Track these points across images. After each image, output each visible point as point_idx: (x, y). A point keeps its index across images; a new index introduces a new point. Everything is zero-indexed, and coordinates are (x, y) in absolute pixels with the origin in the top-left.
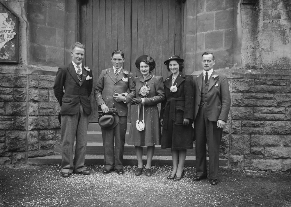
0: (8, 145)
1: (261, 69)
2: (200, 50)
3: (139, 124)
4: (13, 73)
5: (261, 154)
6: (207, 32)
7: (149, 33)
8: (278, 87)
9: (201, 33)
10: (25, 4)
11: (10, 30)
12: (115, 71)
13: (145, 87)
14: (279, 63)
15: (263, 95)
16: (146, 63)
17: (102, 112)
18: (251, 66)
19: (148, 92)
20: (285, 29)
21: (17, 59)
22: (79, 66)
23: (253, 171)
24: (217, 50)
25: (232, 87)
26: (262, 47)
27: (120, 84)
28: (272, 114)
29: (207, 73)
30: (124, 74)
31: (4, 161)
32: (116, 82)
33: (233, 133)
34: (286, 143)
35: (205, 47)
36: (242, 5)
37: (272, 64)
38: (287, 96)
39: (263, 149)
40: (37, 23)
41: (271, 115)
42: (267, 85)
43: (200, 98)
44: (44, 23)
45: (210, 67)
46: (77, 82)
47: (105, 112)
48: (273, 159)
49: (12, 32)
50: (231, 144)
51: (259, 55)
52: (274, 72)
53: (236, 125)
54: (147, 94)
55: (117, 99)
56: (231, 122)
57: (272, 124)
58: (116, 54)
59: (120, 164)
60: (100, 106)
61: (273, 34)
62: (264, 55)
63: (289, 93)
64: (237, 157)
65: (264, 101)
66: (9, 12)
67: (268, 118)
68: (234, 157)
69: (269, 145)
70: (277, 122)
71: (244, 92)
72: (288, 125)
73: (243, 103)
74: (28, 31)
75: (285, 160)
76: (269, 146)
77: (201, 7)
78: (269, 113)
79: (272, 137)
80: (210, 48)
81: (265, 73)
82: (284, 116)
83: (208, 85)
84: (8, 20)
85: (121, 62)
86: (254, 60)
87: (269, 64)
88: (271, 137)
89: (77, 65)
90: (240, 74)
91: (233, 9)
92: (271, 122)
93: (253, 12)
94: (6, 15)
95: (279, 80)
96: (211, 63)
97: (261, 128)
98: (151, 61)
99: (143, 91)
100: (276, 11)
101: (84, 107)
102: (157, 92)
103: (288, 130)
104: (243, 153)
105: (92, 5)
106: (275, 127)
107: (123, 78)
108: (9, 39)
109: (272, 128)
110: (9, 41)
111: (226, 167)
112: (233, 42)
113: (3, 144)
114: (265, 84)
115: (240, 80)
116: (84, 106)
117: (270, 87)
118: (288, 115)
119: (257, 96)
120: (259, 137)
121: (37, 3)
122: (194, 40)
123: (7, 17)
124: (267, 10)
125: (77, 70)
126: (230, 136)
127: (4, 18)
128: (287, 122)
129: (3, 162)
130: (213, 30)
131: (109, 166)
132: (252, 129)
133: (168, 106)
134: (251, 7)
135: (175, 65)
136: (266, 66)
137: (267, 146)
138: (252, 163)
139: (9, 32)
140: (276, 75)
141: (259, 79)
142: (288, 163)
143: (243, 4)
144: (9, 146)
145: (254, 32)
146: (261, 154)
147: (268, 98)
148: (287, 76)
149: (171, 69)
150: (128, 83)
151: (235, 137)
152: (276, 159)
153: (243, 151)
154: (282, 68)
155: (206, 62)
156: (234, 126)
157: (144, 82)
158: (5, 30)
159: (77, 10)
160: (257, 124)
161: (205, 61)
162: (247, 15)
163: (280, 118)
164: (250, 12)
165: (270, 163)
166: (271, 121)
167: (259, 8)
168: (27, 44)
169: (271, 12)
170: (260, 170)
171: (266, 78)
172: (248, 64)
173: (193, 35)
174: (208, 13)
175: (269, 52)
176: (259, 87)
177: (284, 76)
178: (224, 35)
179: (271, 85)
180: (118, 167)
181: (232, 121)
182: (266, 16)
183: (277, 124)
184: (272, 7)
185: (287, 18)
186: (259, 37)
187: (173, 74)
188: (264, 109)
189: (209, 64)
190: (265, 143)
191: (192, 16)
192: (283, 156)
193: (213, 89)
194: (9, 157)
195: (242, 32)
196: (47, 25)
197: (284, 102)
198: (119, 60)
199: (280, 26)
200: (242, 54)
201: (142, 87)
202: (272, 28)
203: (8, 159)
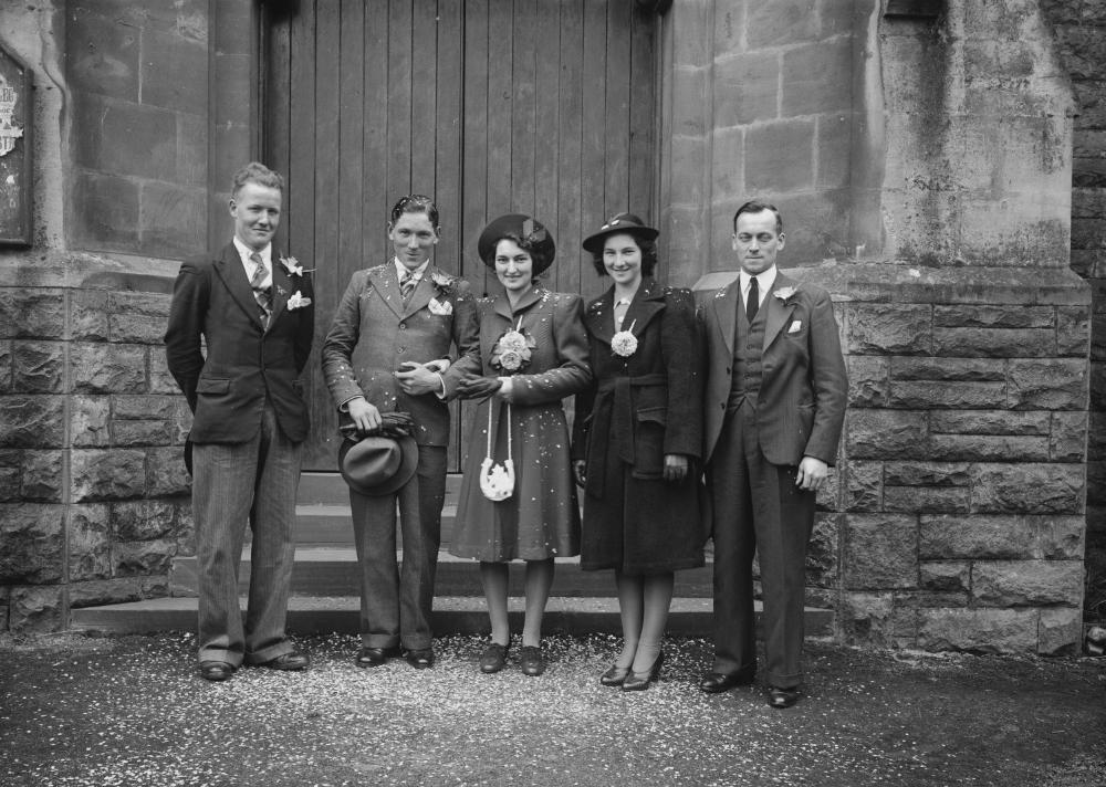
1: (959, 264)
2: (723, 194)
3: (490, 473)
4: (13, 283)
5: (960, 588)
6: (751, 126)
7: (530, 128)
8: (1023, 334)
9: (727, 129)
10: (56, 20)
12: (401, 273)
13: (513, 336)
14: (1028, 241)
15: (965, 365)
16: (519, 245)
17: (356, 429)
18: (918, 255)
19: (527, 355)
20: (1049, 112)
22: (261, 254)
23: (929, 655)
24: (791, 195)
25: (849, 336)
27: (422, 324)
28: (1002, 438)
29: (754, 282)
30: (435, 284)
32: (403, 317)
33: (853, 511)
35: (743, 184)
36: (885, 24)
37: (1000, 248)
38: (1056, 368)
39: (968, 570)
40: (101, 91)
43: (730, 377)
45: (769, 258)
46: (254, 316)
47: (368, 427)
50: (845, 551)
51: (948, 213)
52: (1008, 276)
53: (861, 479)
54: (523, 361)
55: (409, 382)
56: (843, 468)
57: (999, 474)
58: (409, 211)
60: (346, 406)
61: (1003, 130)
62: (970, 211)
63: (1063, 356)
64: (867, 602)
65: (968, 388)
67: (986, 452)
68: (854, 601)
69: (989, 553)
71: (893, 354)
72: (1059, 479)
73: (890, 394)
74: (69, 124)
75: (1048, 611)
77: (729, 29)
78: (988, 434)
80: (765, 187)
81: (972, 282)
82: (1047, 444)
85: (427, 241)
86: (932, 233)
87: (988, 247)
89: (251, 253)
90: (879, 285)
91: (851, 39)
92: (995, 468)
93: (925, 50)
95: (1026, 306)
96: (770, 244)
97: (957, 492)
98: (538, 237)
99: (508, 352)
100: (1014, 46)
102: (562, 355)
103: (1062, 497)
104: (890, 586)
106: (1012, 487)
107: (433, 302)
109: (1002, 491)
111: (828, 639)
112: (850, 163)
114: (971, 322)
115: (879, 307)
116: (279, 410)
117: (991, 334)
119: (941, 370)
120: (952, 524)
122: (703, 157)
124: (982, 41)
125: (250, 269)
126: (841, 520)
128: (1059, 465)
130: (774, 116)
132: (923, 492)
133: (606, 409)
134: (916, 30)
135: (626, 251)
136: (977, 254)
137: (980, 558)
138: (923, 624)
140: (1014, 290)
141: (948, 304)
143: (889, 18)
145: (931, 124)
146: (957, 591)
147: (984, 376)
148: (1055, 290)
150: (451, 321)
151: (859, 524)
153: (890, 578)
154: (1036, 263)
155: (754, 240)
156: (854, 483)
157: (510, 316)
160: (944, 476)
161: (748, 236)
162: (903, 59)
163: (1029, 452)
164: (917, 49)
165: (994, 624)
167: (948, 32)
169: (996, 47)
172: (908, 246)
173: (697, 138)
174: (757, 52)
175: (987, 200)
176: (950, 336)
177: (1045, 291)
179: (996, 325)
180: (414, 642)
181: (846, 464)
182: (976, 63)
183: (1021, 473)
184: (1000, 31)
186: (949, 145)
187: (618, 288)
188: (971, 419)
192: (1043, 597)
196: (140, 99)
197: (1045, 390)
198: (422, 234)
199: (1027, 100)
200: (884, 208)
201: (503, 335)
202: (998, 110)
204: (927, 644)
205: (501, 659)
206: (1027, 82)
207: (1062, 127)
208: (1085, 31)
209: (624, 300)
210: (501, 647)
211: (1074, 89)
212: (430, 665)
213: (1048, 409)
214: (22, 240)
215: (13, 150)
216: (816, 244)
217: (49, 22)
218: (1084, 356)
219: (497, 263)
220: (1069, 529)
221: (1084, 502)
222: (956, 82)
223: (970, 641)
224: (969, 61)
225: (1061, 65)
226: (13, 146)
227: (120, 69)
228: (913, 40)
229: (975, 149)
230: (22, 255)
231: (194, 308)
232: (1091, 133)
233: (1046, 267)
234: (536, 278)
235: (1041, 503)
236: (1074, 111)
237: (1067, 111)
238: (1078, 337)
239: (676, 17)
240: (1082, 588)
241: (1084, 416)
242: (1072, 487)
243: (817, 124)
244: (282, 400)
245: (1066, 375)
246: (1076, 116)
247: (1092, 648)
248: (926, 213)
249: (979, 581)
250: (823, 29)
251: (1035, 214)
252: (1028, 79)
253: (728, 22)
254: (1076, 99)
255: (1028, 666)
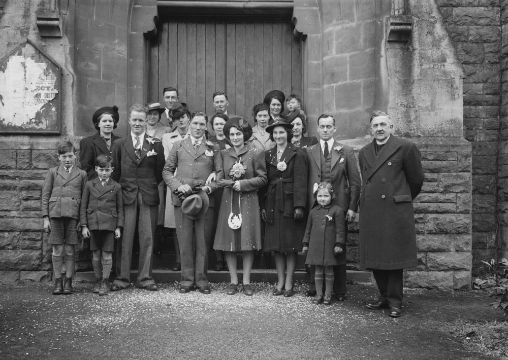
0: (47, 253)
1: (419, 136)
3: (232, 218)
4: (54, 148)
6: (337, 84)
7: (252, 86)
8: (445, 163)
9: (328, 85)
11: (50, 87)
13: (238, 165)
14: (446, 127)
16: (238, 129)
18: (403, 133)
19: (243, 172)
20: (453, 77)
21: (60, 129)
22: (139, 137)
23: (409, 289)
24: (353, 111)
26: (419, 105)
27: (203, 160)
29: (326, 143)
30: (207, 145)
31: (41, 276)
34: (459, 246)
35: (335, 107)
36: (388, 44)
37: (435, 130)
38: (457, 176)
39: (425, 256)
40: (87, 75)
41: (435, 205)
42: (428, 160)
43: (320, 178)
44: (98, 74)
45: (331, 135)
46: (134, 160)
48: (440, 271)
49: (52, 90)
51: (414, 117)
54: (242, 174)
58: (198, 115)
59: (204, 279)
61: (435, 84)
62: (423, 116)
63: (461, 172)
66: (47, 60)
67: (431, 209)
69: (433, 249)
70: (444, 216)
74: (75, 88)
75: (457, 272)
76: (434, 251)
77: (329, 47)
78: (432, 202)
79: (438, 238)
80: (342, 108)
81: (424, 143)
83: (329, 160)
84: (46, 73)
85: (142, 124)
86: (408, 125)
87: (430, 130)
88: (436, 238)
89: (135, 136)
91: (375, 50)
92: (435, 215)
94: (44, 65)
95: (445, 152)
96: (331, 129)
97: (420, 225)
98: (245, 126)
99: (236, 171)
101: (144, 195)
105: (166, 46)
106: (441, 223)
107: (207, 151)
108: (48, 99)
109: (437, 224)
110: (47, 102)
111: (369, 284)
113: (39, 252)
117: (432, 163)
118: (460, 205)
121: (88, 48)
122: (320, 96)
123: (45, 68)
125: (135, 142)
127: (40, 69)
128: (460, 215)
129: (40, 278)
130: (346, 80)
131: (188, 282)
133: (274, 190)
135: (281, 132)
136: (426, 132)
137: (430, 251)
138: (408, 277)
139: (48, 90)
140: (441, 146)
142: (463, 276)
144: (47, 255)
145: (407, 83)
146: (420, 264)
147: (429, 180)
148: (457, 146)
149: (276, 138)
150: (213, 158)
152: (445, 270)
155: (325, 127)
157: (236, 157)
158: (42, 87)
159: (145, 57)
161: (323, 126)
162: (395, 58)
165: (435, 277)
166: (435, 214)
167: (412, 47)
168: (74, 106)
169: (432, 52)
170: (421, 287)
171: (425, 150)
173: (317, 89)
174: (339, 56)
177: (453, 146)
178: (362, 87)
179: (433, 160)
180: (201, 284)
182: (424, 58)
183: (445, 218)
185: (456, 61)
186: (414, 90)
187: (278, 146)
188: (425, 196)
189: (329, 130)
190: (427, 246)
191: (317, 60)
192: (454, 266)
193: (338, 166)
194: (47, 270)
195: (389, 83)
196: (101, 78)
197: (453, 185)
198: (202, 124)
199: (445, 73)
201: (234, 164)
202: (433, 77)
203: (46, 273)
204: (409, 285)
205: (235, 290)
206: (444, 65)
207: (458, 83)
208: (470, 45)
209: (281, 151)
210: (235, 285)
211: (463, 68)
212: (209, 292)
213: (455, 192)
214: (57, 132)
215: (55, 98)
216: (363, 129)
217: (68, 50)
218: (469, 171)
219: (230, 136)
220: (465, 240)
221: (471, 229)
222: (416, 66)
223: (426, 284)
224: (421, 58)
225: (458, 59)
226: (54, 97)
227: (94, 67)
228: (398, 50)
229: (424, 91)
230: (58, 137)
231: (117, 158)
232: (474, 84)
233: (454, 137)
234: (246, 142)
235: (453, 229)
236: (463, 76)
237: (461, 76)
238: (467, 164)
239: (308, 42)
240: (471, 263)
241: (470, 195)
242: (465, 223)
243: (362, 83)
244: (145, 190)
245: (462, 179)
246: (464, 78)
247: (476, 287)
248: (406, 117)
249: (429, 260)
250: (364, 46)
251: (449, 116)
252: (445, 64)
253: (328, 44)
254: (464, 71)
255: (448, 293)
